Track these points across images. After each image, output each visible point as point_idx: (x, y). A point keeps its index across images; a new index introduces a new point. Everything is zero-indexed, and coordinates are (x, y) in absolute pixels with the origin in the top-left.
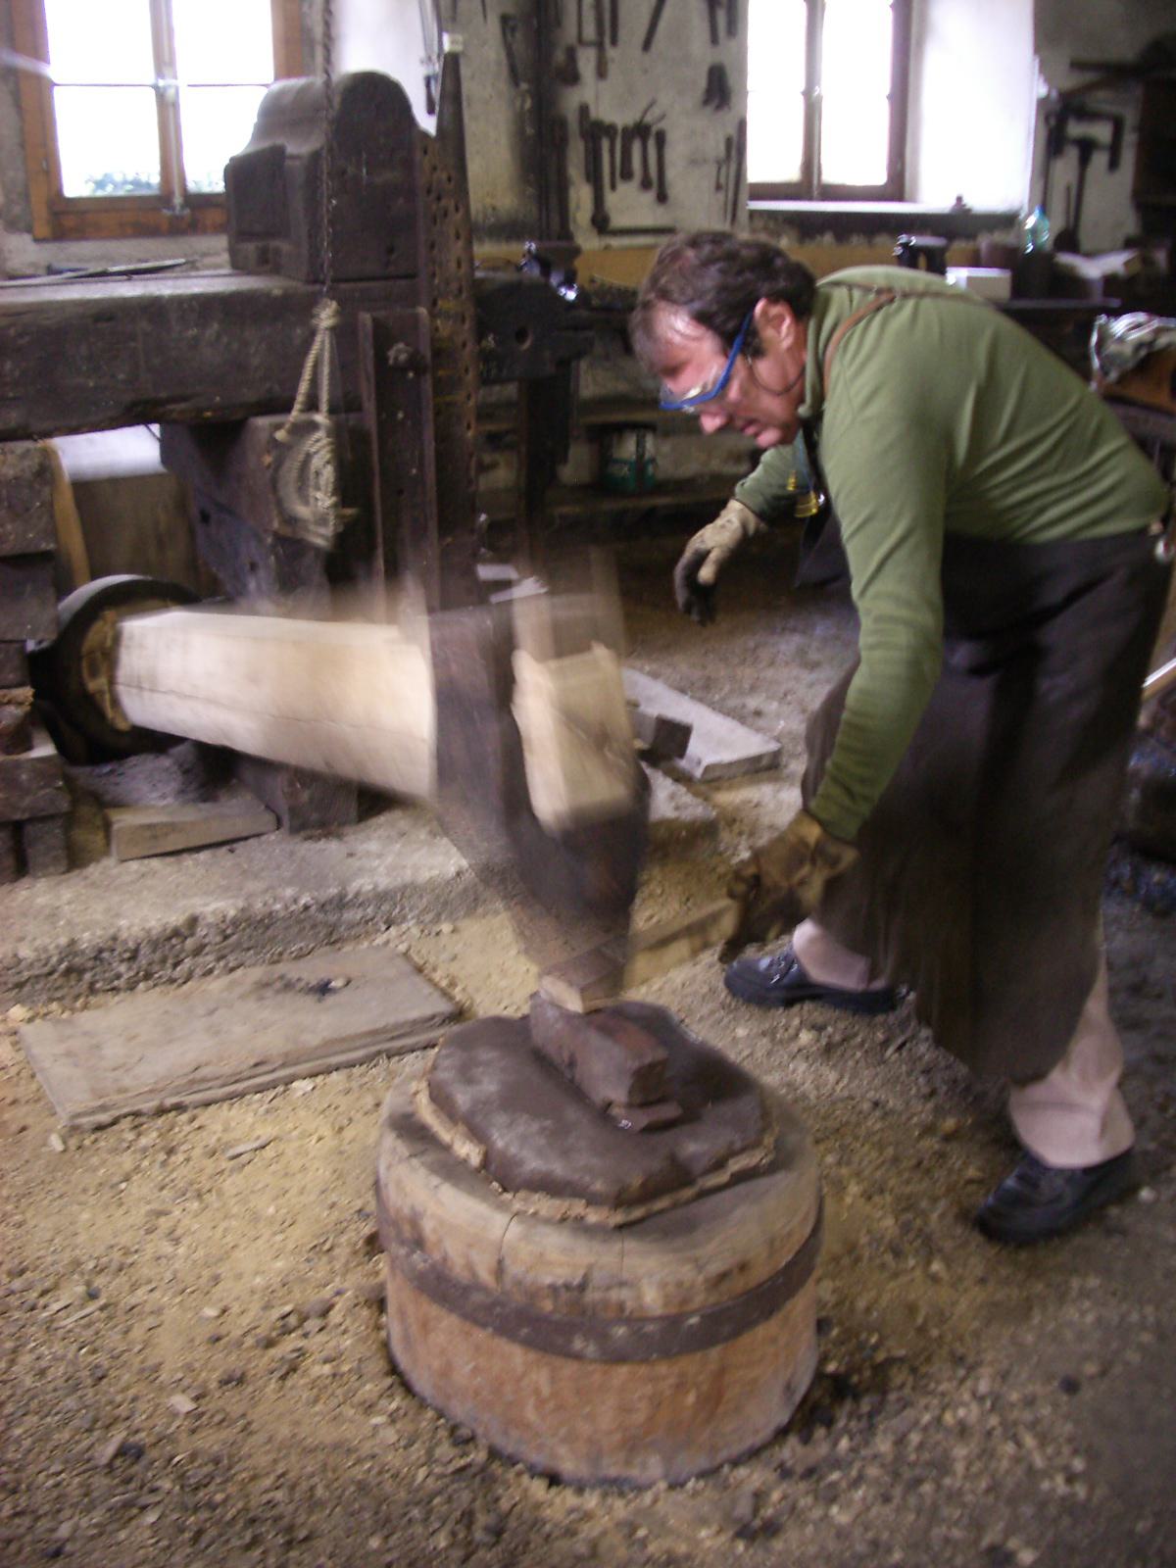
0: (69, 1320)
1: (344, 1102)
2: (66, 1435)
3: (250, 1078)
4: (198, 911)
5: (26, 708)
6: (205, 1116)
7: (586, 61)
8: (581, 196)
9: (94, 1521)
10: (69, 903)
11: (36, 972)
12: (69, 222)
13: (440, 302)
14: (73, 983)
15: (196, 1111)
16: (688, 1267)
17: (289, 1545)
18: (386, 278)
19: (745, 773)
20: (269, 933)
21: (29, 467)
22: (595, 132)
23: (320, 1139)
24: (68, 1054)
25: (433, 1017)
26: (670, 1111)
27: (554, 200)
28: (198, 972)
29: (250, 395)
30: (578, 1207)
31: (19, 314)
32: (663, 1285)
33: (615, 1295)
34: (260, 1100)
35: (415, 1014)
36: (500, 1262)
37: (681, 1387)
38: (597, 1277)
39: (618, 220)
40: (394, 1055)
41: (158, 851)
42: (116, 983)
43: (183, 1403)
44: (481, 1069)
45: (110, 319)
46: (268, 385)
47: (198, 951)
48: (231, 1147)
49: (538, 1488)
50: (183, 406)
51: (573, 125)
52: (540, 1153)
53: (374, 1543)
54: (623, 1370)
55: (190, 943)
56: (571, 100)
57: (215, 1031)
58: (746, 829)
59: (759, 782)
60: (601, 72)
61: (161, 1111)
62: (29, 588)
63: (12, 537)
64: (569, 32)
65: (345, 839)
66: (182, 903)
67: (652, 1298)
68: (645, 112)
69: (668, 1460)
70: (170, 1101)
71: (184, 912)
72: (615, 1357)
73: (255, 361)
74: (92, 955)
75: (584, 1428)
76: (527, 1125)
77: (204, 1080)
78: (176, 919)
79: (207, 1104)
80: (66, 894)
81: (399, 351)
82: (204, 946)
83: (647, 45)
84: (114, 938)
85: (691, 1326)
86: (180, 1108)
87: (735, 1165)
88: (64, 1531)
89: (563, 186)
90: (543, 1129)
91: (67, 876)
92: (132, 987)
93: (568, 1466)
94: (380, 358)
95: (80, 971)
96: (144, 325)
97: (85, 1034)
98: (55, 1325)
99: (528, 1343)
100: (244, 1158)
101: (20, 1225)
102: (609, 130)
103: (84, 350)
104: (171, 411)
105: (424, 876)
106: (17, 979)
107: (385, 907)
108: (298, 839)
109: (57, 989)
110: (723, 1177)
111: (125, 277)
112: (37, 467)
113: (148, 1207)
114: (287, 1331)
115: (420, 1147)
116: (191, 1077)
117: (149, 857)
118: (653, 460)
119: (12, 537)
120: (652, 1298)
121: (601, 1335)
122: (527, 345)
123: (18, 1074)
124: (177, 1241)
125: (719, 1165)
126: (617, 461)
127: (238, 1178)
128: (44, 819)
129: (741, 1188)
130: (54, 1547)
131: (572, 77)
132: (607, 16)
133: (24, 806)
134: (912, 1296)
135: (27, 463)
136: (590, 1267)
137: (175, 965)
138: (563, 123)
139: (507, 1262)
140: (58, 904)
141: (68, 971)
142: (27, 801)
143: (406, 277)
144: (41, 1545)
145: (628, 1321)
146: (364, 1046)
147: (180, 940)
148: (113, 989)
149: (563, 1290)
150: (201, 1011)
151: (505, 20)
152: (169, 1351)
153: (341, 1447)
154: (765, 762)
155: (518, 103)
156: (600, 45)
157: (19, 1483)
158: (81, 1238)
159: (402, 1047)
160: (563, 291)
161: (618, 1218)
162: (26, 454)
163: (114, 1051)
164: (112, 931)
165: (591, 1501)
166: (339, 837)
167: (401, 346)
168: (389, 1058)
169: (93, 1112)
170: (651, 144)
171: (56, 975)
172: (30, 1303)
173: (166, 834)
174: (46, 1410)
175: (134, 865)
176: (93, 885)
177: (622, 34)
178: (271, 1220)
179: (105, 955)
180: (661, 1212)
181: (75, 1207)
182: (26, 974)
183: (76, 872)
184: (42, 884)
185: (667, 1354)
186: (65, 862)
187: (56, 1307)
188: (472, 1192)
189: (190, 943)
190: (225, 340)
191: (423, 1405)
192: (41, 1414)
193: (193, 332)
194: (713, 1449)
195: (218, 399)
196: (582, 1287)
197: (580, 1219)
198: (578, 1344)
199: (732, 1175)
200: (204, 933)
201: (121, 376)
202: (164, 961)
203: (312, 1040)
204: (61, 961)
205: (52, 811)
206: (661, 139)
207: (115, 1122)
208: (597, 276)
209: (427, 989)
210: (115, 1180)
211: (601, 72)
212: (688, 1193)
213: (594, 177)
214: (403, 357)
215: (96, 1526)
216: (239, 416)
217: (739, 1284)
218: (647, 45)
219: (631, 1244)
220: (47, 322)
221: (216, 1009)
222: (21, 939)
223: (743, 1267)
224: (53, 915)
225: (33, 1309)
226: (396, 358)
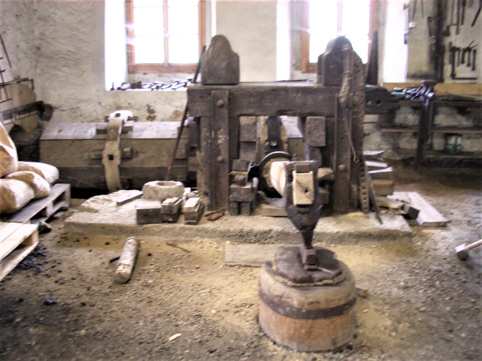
7: (453, 30)
8: (448, 69)
12: (311, 68)
16: (303, 298)
17: (217, 336)
19: (435, 226)
20: (288, 237)
22: (454, 50)
24: (232, 251)
27: (439, 69)
29: (308, 111)
30: (286, 280)
32: (298, 300)
37: (301, 327)
39: (459, 75)
42: (250, 241)
47: (271, 237)
49: (271, 344)
51: (447, 47)
53: (232, 341)
55: (269, 235)
56: (447, 41)
57: (266, 254)
59: (438, 229)
60: (457, 32)
61: (245, 266)
64: (448, 22)
67: (295, 303)
68: (470, 45)
69: (298, 345)
70: (248, 264)
72: (287, 315)
75: (281, 332)
77: (257, 262)
78: (267, 229)
79: (256, 267)
82: (272, 237)
83: (473, 24)
85: (303, 312)
86: (250, 266)
87: (325, 281)
89: (442, 65)
92: (255, 242)
93: (278, 340)
102: (458, 49)
105: (329, 231)
107: (318, 237)
114: (241, 306)
120: (295, 303)
121: (284, 308)
125: (321, 280)
126: (449, 144)
131: (447, 34)
132: (461, 17)
133: (241, 198)
136: (284, 292)
138: (443, 47)
141: (240, 236)
145: (290, 306)
148: (250, 242)
151: (429, 18)
153: (239, 327)
154: (442, 224)
155: (431, 41)
156: (457, 24)
161: (293, 284)
162: (251, 119)
163: (242, 252)
165: (280, 349)
169: (230, 262)
170: (472, 53)
171: (237, 236)
175: (265, 217)
177: (466, 21)
179: (249, 234)
180: (303, 286)
185: (298, 318)
189: (269, 235)
193: (294, 95)
194: (309, 347)
197: (286, 283)
204: (239, 232)
206: (475, 52)
210: (228, 275)
211: (457, 32)
212: (312, 284)
213: (452, 62)
217: (316, 306)
218: (473, 24)
222: (232, 226)
224: (241, 223)
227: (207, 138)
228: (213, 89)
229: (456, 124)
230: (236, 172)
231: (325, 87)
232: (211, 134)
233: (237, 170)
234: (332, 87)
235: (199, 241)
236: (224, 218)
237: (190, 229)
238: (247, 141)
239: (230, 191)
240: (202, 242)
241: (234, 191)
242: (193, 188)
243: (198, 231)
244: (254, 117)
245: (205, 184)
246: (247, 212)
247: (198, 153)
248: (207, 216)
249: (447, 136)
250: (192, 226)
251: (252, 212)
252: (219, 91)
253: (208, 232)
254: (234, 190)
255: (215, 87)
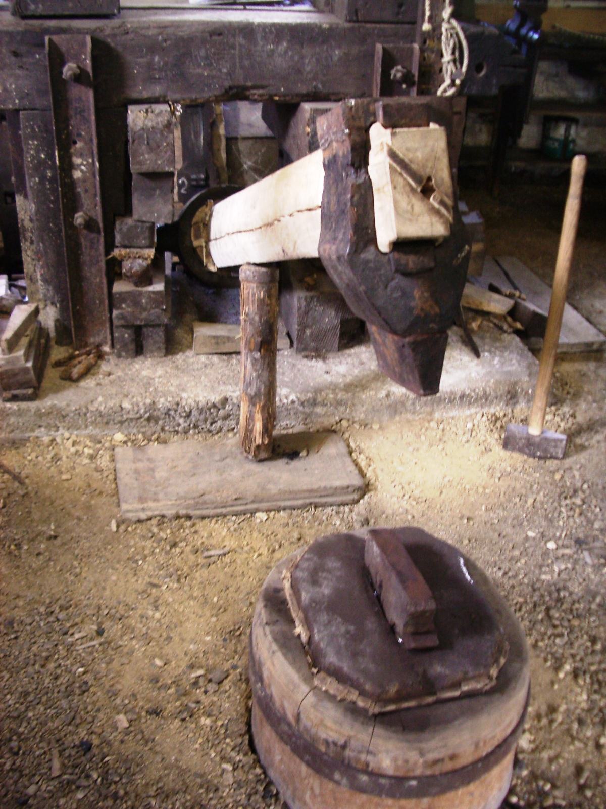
0: (80, 647)
1: (281, 532)
2: (57, 723)
3: (232, 506)
4: (229, 395)
5: (149, 262)
6: (200, 525)
9: (49, 788)
10: (160, 377)
11: (131, 416)
13: (428, 42)
14: (151, 425)
15: (195, 521)
18: (398, 23)
21: (161, 122)
23: (260, 555)
25: (348, 487)
26: (432, 641)
28: (225, 429)
29: (303, 89)
30: (354, 696)
31: (166, 27)
33: (363, 757)
34: (235, 522)
35: (338, 483)
36: (299, 714)
38: (353, 743)
40: (319, 507)
41: (219, 351)
43: (122, 721)
44: (324, 575)
45: (220, 34)
46: (314, 83)
48: (208, 550)
50: (261, 91)
52: (338, 653)
54: (364, 797)
55: (221, 412)
57: (221, 471)
58: (572, 391)
61: (178, 517)
62: (158, 192)
63: (148, 162)
65: (327, 361)
66: (222, 388)
70: (183, 512)
71: (221, 394)
73: (308, 68)
74: (164, 412)
76: (340, 627)
78: (215, 398)
80: (160, 371)
81: (398, 71)
84: (178, 404)
86: (189, 517)
88: (32, 790)
90: (348, 632)
91: (164, 359)
94: (385, 73)
95: (157, 420)
96: (241, 40)
97: (149, 460)
98: (72, 648)
99: (308, 764)
100: (213, 559)
101: (77, 576)
103: (203, 53)
104: (255, 94)
106: (119, 418)
108: (300, 357)
109: (142, 427)
110: (457, 693)
111: (242, 7)
112: (166, 122)
113: (149, 580)
115: (275, 617)
116: (197, 500)
117: (213, 354)
118: (573, 141)
119: (148, 162)
122: (482, 74)
123: (107, 477)
124: (156, 608)
125: (456, 685)
127: (205, 572)
128: (153, 326)
129: (465, 702)
130: (23, 799)
134: (582, 760)
135: (160, 119)
136: (350, 738)
137: (212, 424)
139: (302, 716)
140: (153, 376)
142: (145, 315)
143: (408, 23)
144: (18, 795)
146: (304, 498)
147: (215, 410)
149: (331, 745)
150: (217, 457)
152: (128, 682)
154: (595, 347)
157: (19, 749)
158: (107, 593)
159: (326, 503)
160: (531, 34)
164: (177, 399)
166: (324, 359)
167: (399, 67)
168: (315, 507)
171: (142, 420)
172: (65, 630)
173: (224, 343)
174: (50, 704)
176: (177, 367)
178: (213, 606)
181: (110, 571)
182: (125, 417)
183: (170, 357)
184: (149, 362)
186: (164, 351)
187: (77, 636)
188: (293, 663)
190: (290, 53)
191: (258, 761)
192: (47, 706)
195: (282, 89)
196: (344, 747)
198: (337, 776)
199: (462, 692)
200: (231, 407)
201: (225, 70)
202: (205, 420)
203: (273, 489)
204: (146, 412)
205: (157, 322)
207: (150, 519)
208: (557, 25)
209: (352, 467)
212: (430, 699)
214: (399, 75)
215: (50, 792)
216: (295, 101)
217: (449, 766)
219: (379, 730)
220: (180, 34)
221: (227, 457)
223: (453, 757)
224: (148, 383)
225: (66, 633)
226: (395, 76)
227: (40, 167)
228: (47, 31)
229: (563, 94)
230: (123, 252)
231: (347, 25)
232: (51, 156)
233: (125, 247)
234: (368, 26)
235: (46, 439)
236: (105, 367)
237: (20, 413)
238: (151, 170)
239: (112, 301)
240: (53, 440)
241: (123, 300)
242: (14, 276)
243: (39, 415)
244: (165, 108)
245: (45, 280)
246: (159, 348)
247: (28, 445)
248: (58, 364)
249: (548, 122)
250: (24, 405)
251: (171, 347)
252: (68, 36)
253: (64, 417)
254: (123, 297)
255: (52, 23)
